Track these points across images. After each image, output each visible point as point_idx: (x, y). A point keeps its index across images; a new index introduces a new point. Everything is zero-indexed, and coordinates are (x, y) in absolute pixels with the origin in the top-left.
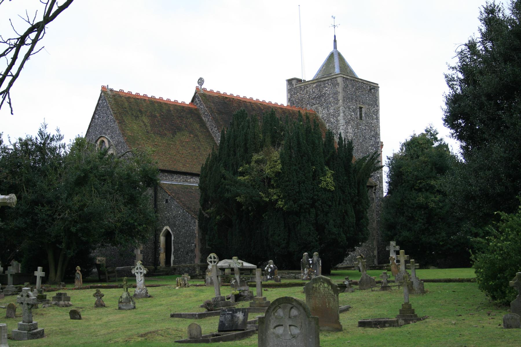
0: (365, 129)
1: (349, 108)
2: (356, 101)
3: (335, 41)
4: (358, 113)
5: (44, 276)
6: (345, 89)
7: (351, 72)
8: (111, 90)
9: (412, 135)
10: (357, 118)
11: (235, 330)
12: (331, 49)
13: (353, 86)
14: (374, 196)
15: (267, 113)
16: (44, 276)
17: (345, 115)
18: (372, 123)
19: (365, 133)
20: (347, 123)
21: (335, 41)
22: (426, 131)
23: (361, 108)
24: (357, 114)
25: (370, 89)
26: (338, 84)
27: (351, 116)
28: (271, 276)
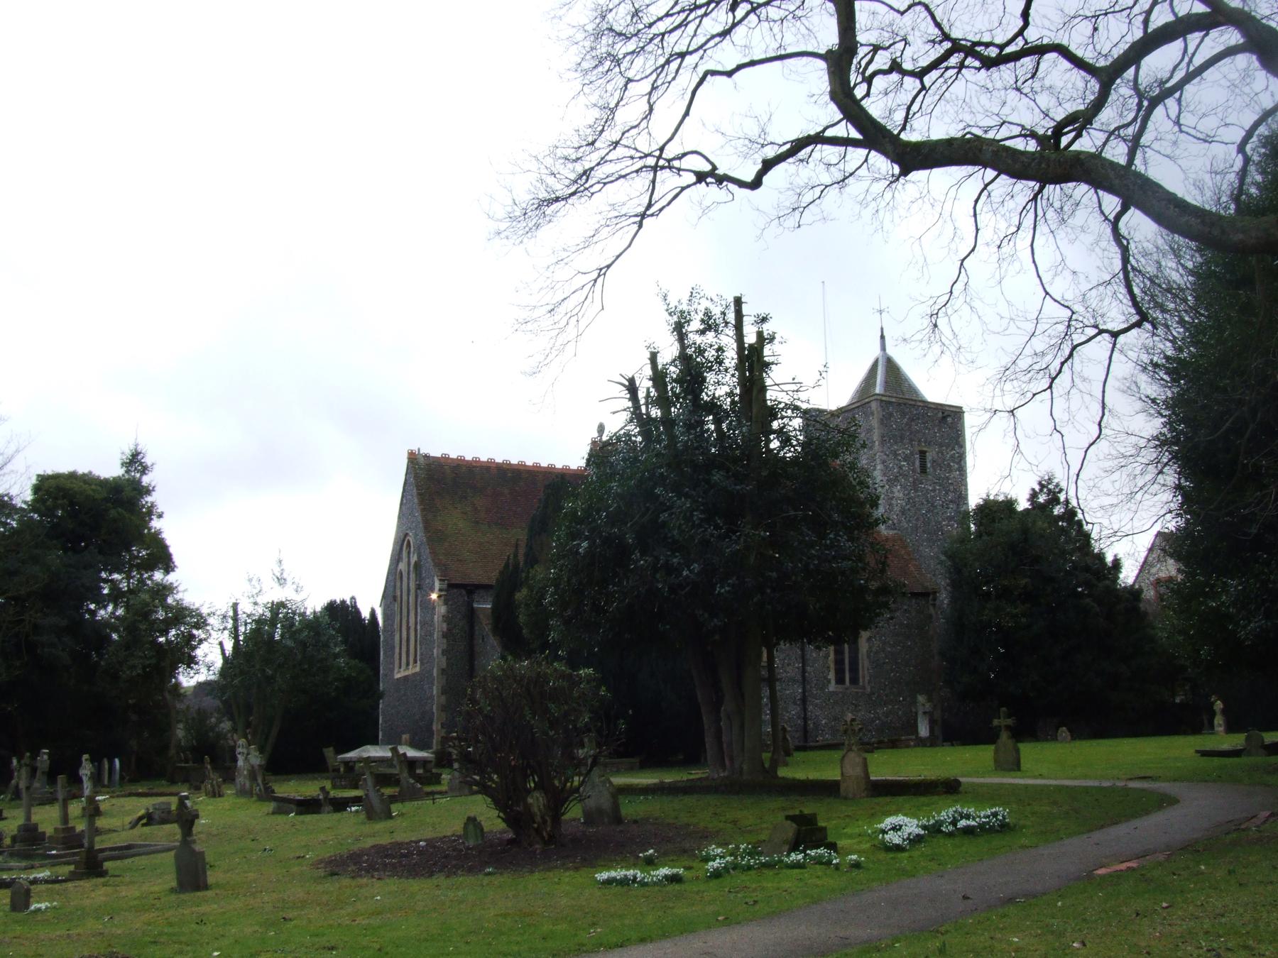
0: (934, 490)
1: (896, 455)
2: (911, 440)
3: (882, 337)
4: (917, 463)
5: (331, 749)
6: (884, 421)
7: (912, 389)
8: (426, 457)
9: (984, 496)
10: (914, 471)
11: (1035, 777)
12: (876, 352)
13: (903, 414)
14: (932, 610)
15: (554, 483)
16: (331, 749)
17: (887, 467)
18: (948, 478)
19: (933, 497)
20: (892, 482)
21: (882, 337)
22: (1040, 483)
23: (923, 453)
24: (914, 464)
25: (944, 418)
26: (872, 414)
27: (900, 468)
28: (579, 774)
